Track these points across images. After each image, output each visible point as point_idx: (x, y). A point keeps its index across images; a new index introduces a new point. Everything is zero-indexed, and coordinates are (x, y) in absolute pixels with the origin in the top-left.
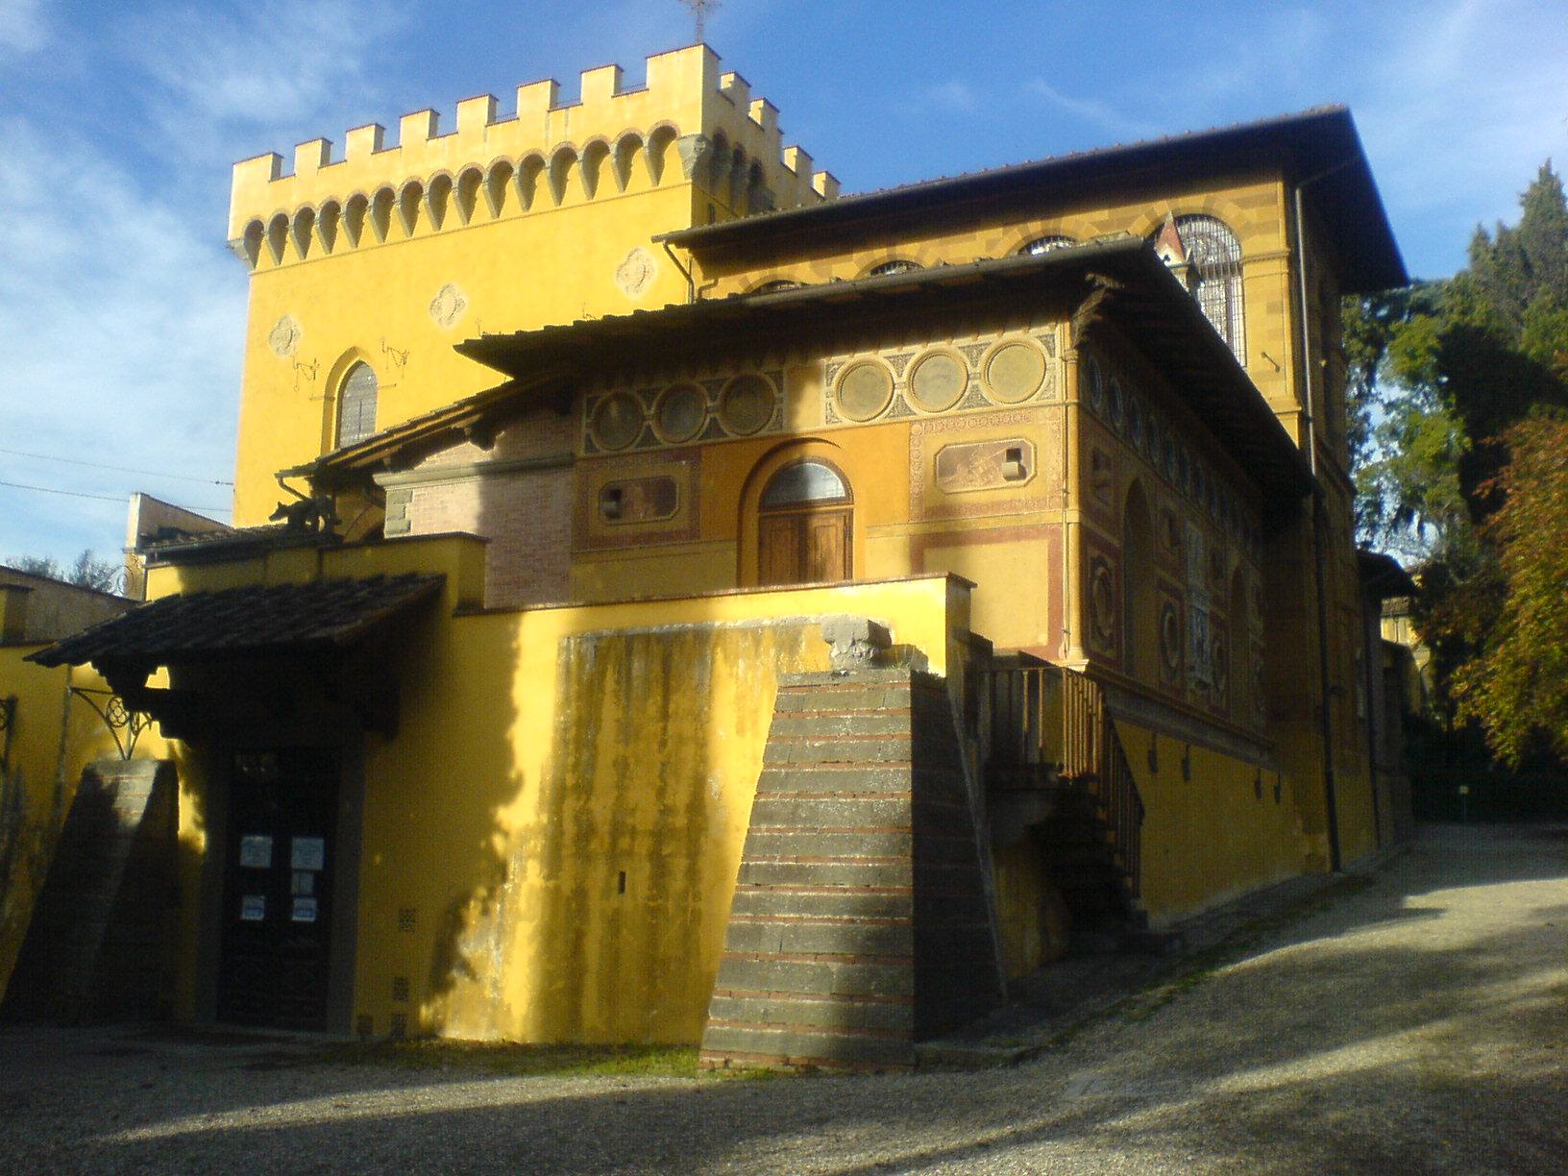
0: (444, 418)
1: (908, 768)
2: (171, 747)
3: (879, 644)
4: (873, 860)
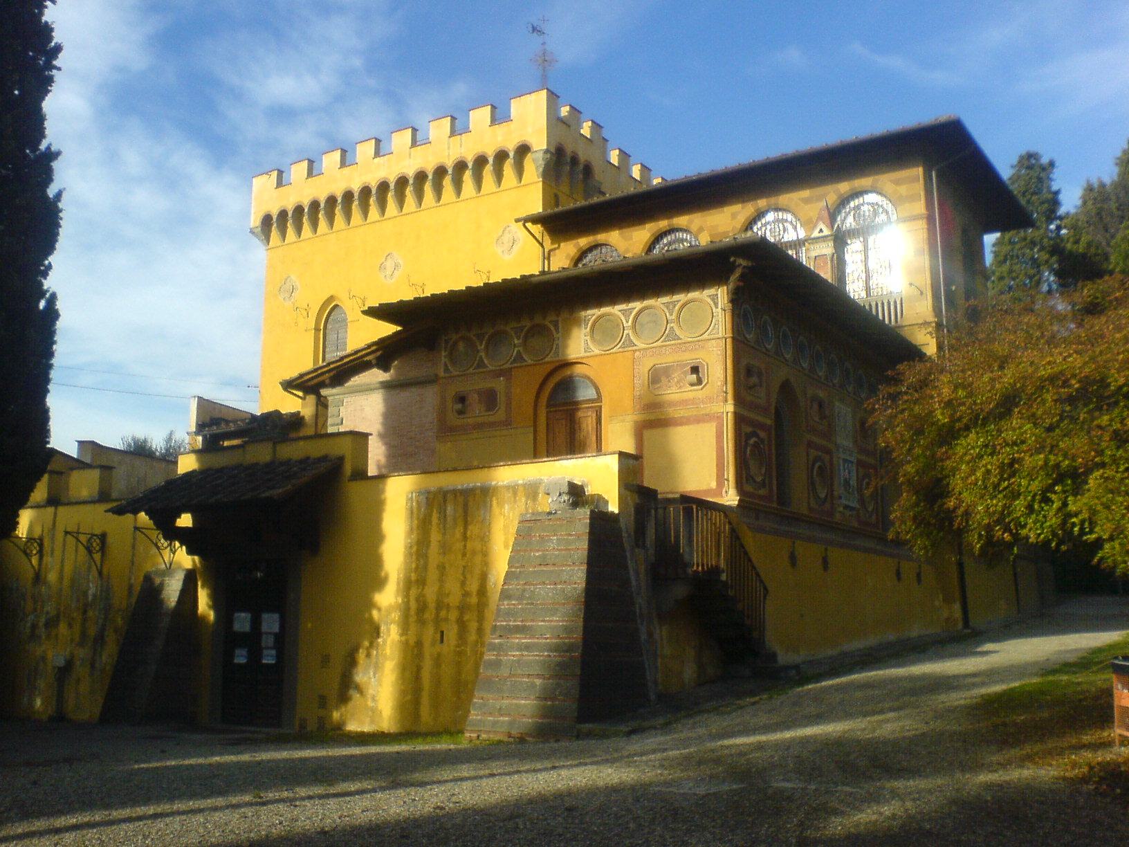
0: (359, 355)
1: (584, 567)
2: (194, 561)
3: (576, 493)
4: (563, 621)
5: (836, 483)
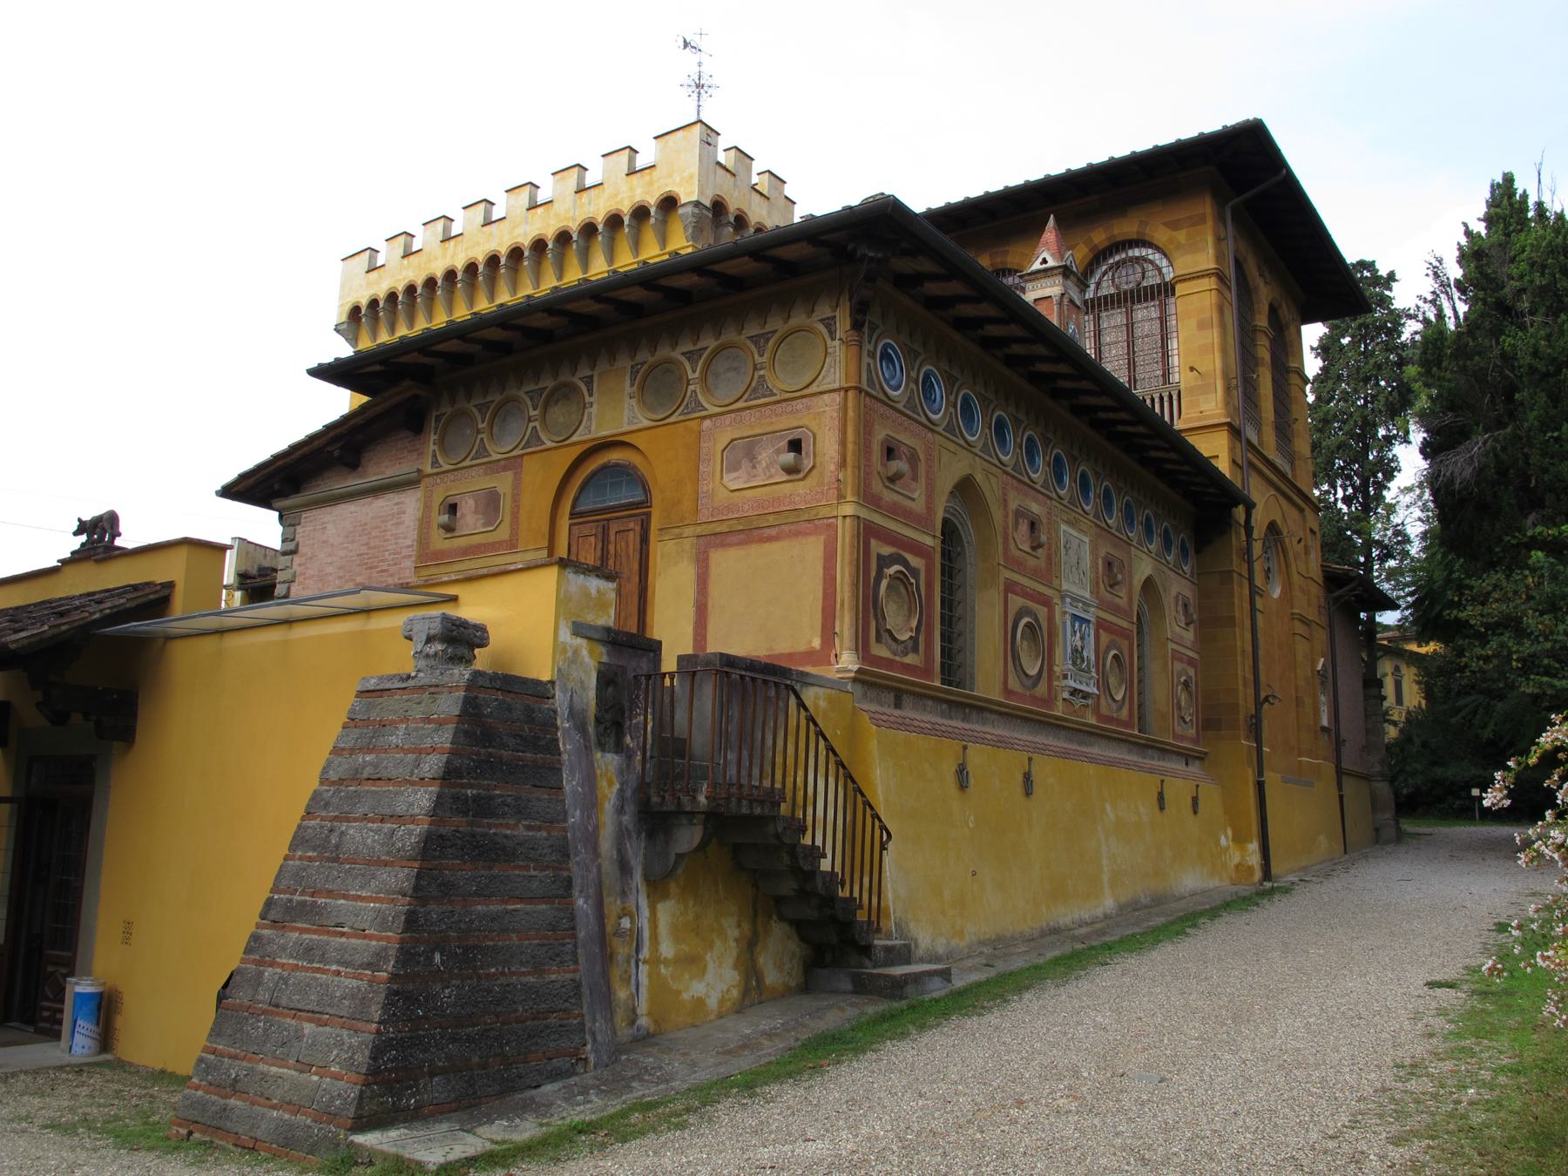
5: (1058, 652)
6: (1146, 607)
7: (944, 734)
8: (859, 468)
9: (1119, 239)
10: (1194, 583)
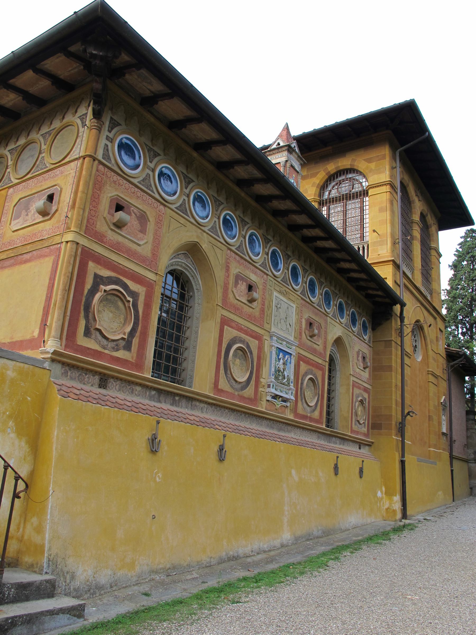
5: (265, 372)
6: (338, 355)
7: (145, 411)
8: (84, 210)
9: (341, 168)
10: (370, 346)
